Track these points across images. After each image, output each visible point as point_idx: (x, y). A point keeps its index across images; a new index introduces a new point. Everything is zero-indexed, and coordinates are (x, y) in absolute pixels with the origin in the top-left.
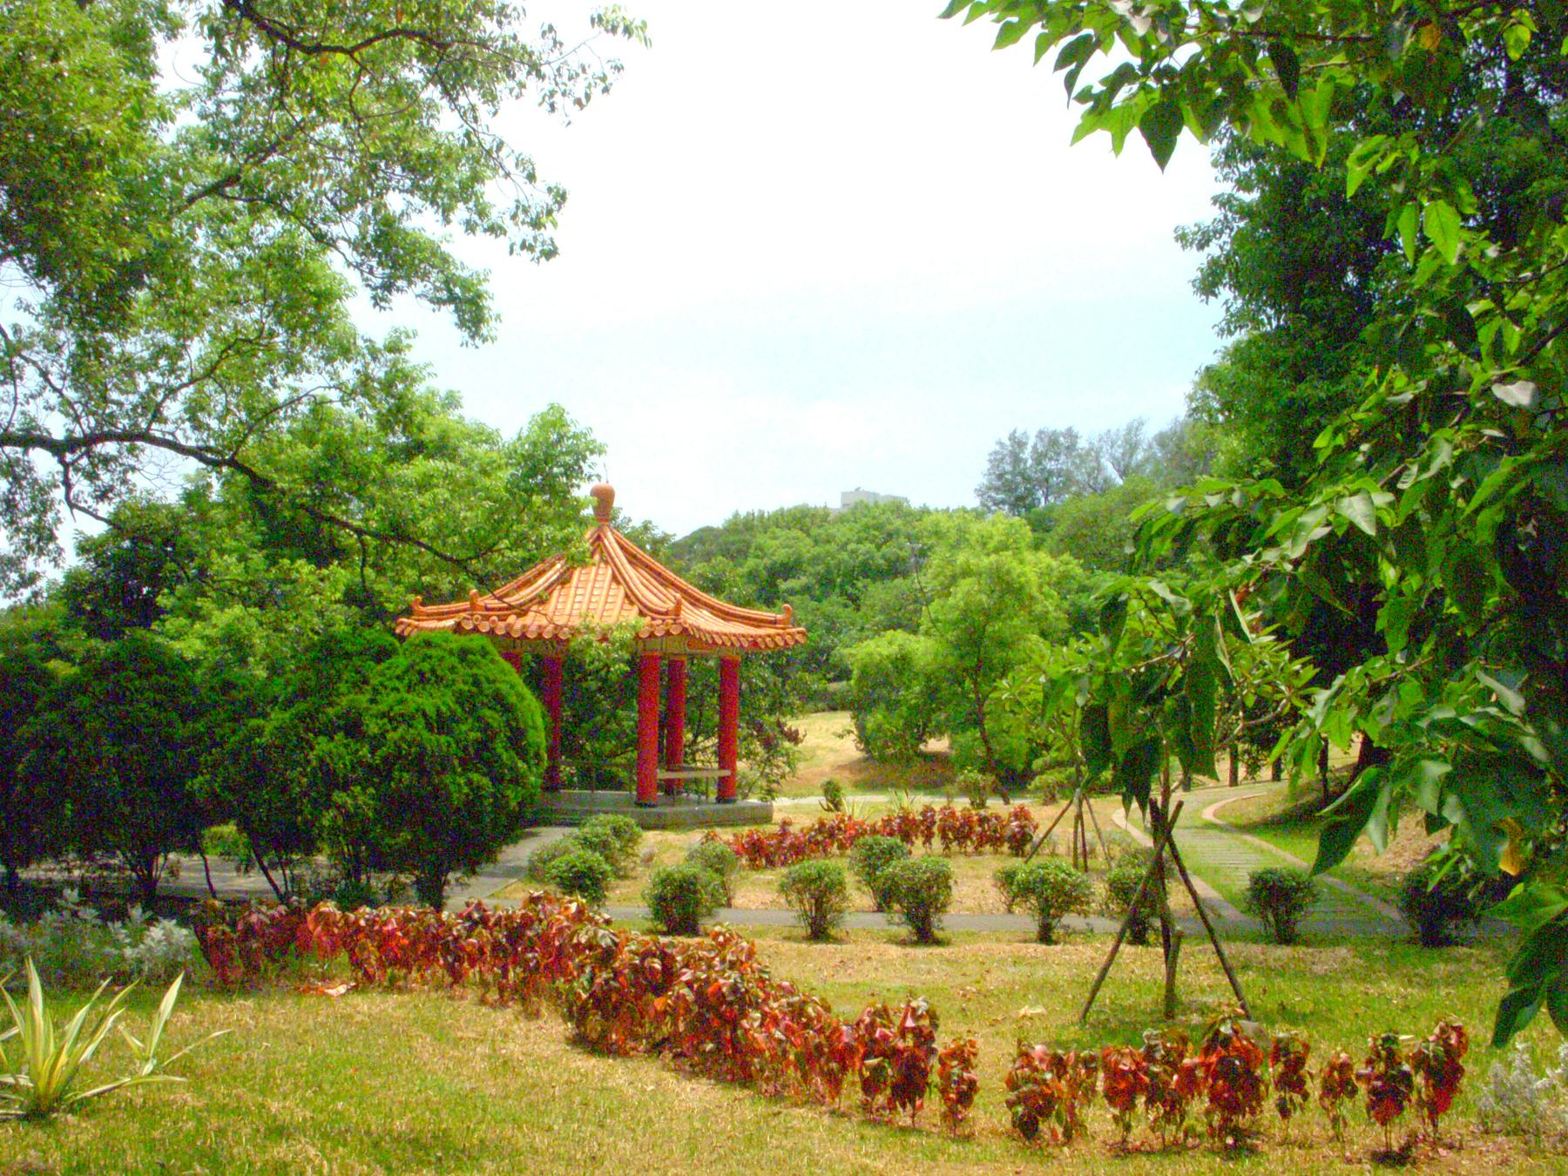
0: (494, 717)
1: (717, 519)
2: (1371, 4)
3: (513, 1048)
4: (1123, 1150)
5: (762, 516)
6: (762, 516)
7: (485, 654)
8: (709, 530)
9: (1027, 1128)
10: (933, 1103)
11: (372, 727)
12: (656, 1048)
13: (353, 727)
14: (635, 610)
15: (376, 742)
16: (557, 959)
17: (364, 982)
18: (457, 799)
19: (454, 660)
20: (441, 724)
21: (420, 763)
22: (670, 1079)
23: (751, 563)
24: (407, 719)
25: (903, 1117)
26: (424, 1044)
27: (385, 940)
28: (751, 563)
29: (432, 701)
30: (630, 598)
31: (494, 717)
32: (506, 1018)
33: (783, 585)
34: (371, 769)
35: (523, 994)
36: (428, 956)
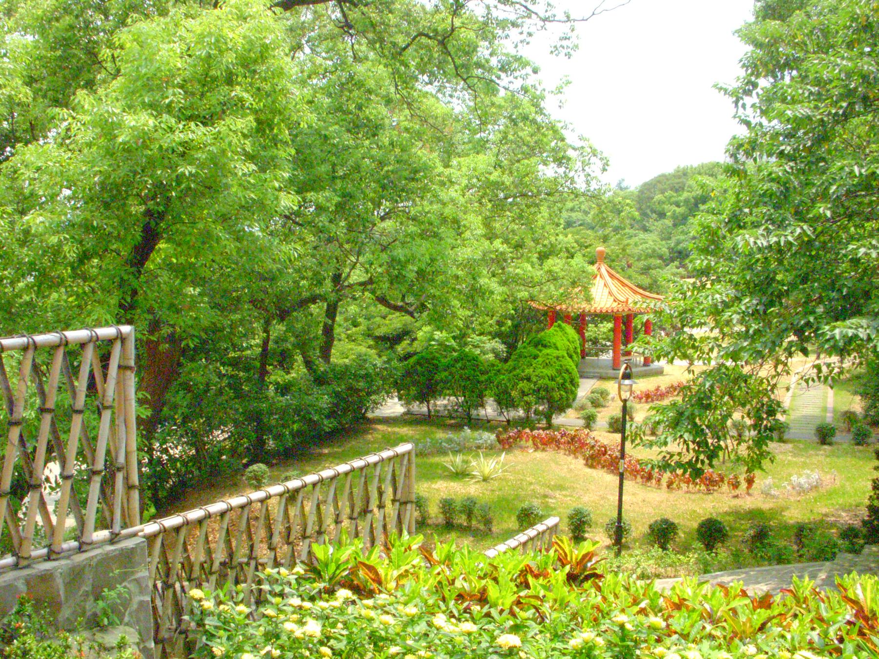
0: (566, 376)
1: (669, 169)
2: (877, 100)
3: (572, 466)
4: (687, 492)
5: (692, 167)
6: (692, 167)
7: (563, 357)
8: (663, 176)
9: (668, 487)
10: (654, 481)
11: (534, 379)
12: (603, 467)
13: (529, 379)
14: (612, 299)
15: (535, 383)
16: (583, 445)
17: (537, 448)
18: (557, 399)
19: (555, 360)
20: (552, 379)
21: (546, 389)
22: (605, 474)
23: (685, 195)
24: (543, 377)
25: (649, 484)
26: (553, 465)
27: (542, 439)
28: (685, 195)
29: (549, 372)
30: (610, 293)
31: (566, 376)
32: (570, 458)
33: (702, 207)
34: (534, 391)
35: (574, 452)
36: (552, 442)
